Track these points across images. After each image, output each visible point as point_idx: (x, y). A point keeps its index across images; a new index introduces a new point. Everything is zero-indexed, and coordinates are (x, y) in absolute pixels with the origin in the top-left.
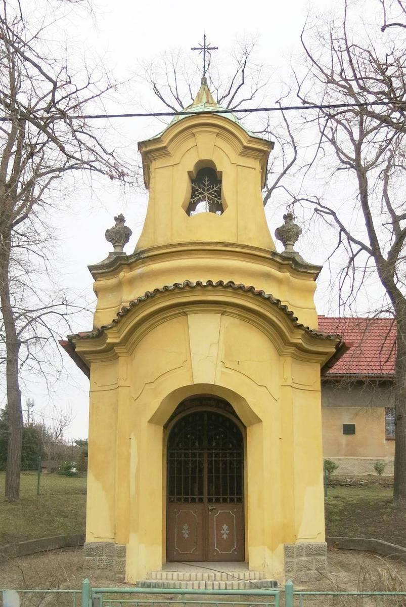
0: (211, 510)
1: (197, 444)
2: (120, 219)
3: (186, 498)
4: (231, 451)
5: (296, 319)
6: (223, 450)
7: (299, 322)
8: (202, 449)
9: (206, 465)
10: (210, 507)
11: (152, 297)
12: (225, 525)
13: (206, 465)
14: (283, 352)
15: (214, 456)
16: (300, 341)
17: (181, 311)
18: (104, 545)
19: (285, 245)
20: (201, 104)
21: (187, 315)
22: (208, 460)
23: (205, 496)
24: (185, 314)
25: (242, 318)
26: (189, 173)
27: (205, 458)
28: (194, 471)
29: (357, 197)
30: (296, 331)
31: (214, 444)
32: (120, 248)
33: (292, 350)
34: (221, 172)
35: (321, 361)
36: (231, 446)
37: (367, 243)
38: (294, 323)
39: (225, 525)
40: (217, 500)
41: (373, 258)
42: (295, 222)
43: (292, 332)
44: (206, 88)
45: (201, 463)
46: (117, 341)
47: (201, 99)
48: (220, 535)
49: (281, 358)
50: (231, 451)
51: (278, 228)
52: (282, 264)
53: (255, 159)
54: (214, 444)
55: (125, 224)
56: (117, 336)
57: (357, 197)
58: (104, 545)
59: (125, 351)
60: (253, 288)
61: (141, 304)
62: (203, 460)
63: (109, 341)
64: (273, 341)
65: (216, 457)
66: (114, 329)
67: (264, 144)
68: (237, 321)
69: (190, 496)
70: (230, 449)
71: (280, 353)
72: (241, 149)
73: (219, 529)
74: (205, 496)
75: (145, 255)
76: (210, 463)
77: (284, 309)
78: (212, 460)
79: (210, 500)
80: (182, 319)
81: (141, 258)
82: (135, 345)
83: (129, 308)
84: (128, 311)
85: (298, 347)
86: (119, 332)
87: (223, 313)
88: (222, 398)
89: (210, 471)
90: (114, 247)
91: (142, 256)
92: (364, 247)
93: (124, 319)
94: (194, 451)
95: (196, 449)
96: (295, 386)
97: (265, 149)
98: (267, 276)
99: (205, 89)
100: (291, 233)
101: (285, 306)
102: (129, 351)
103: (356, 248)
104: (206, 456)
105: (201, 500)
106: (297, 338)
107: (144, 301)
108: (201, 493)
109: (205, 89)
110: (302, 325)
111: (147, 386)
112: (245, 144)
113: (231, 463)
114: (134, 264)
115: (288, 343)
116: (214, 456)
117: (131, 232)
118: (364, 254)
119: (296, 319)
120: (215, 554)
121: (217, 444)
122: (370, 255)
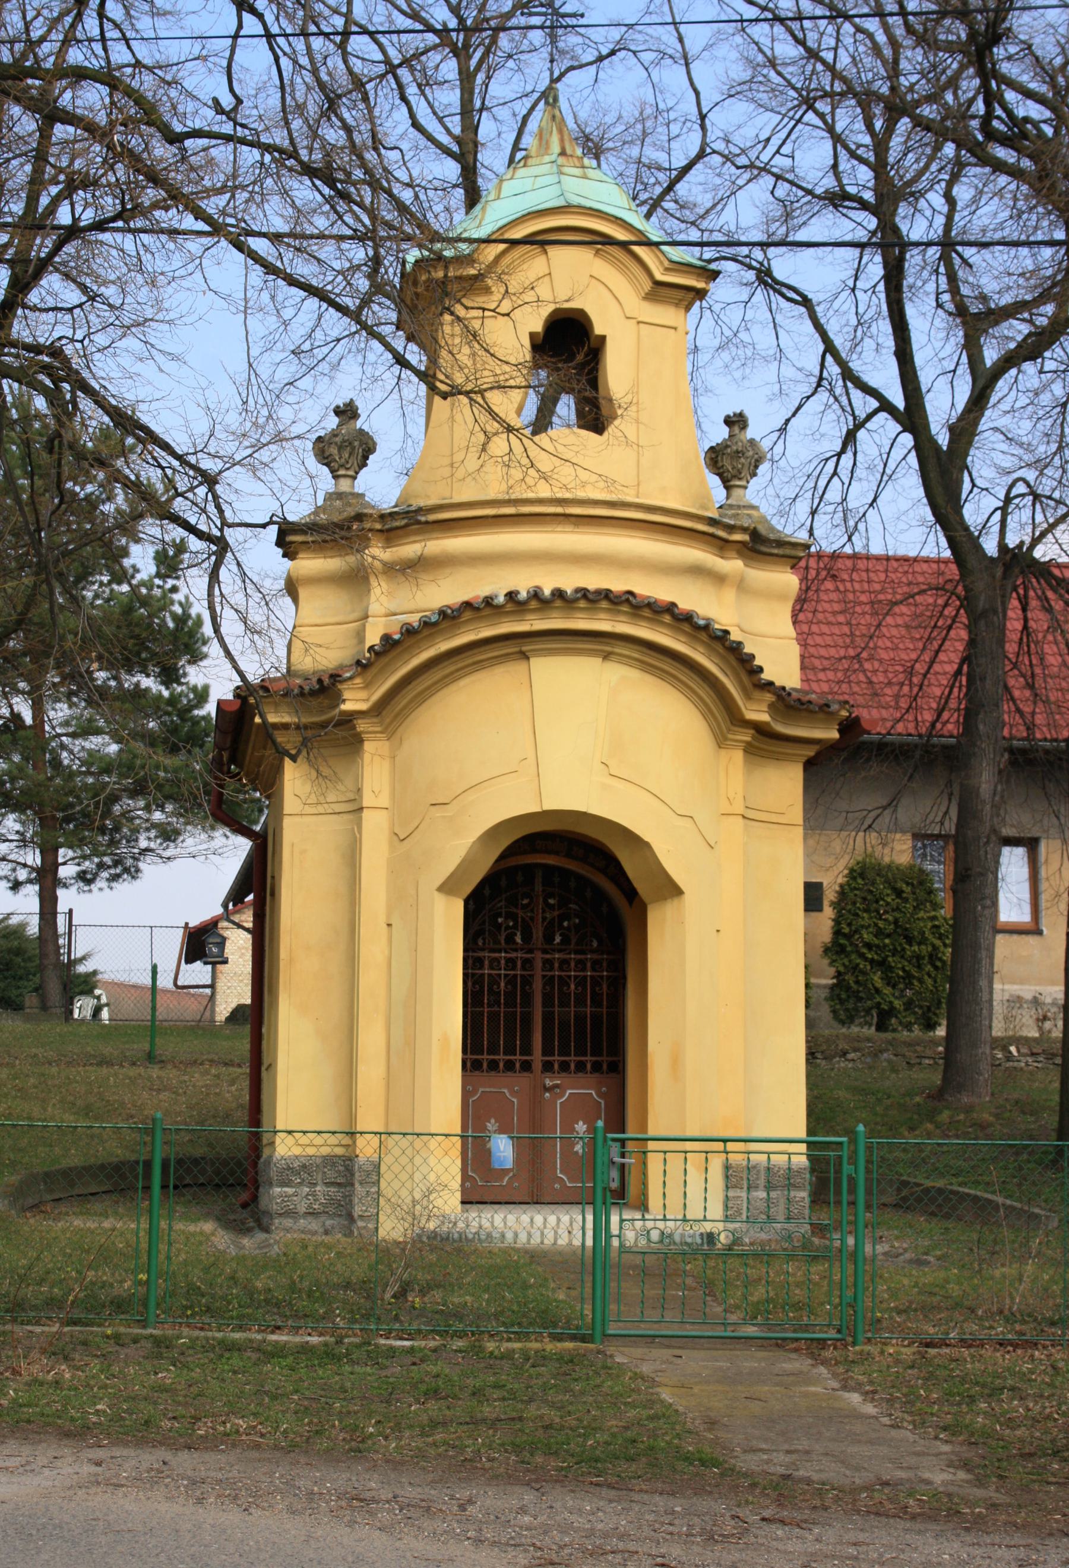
0: (547, 1089)
1: (518, 939)
2: (347, 412)
3: (509, 1061)
4: (595, 956)
5: (761, 669)
6: (576, 952)
7: (766, 676)
8: (530, 951)
9: (538, 986)
10: (548, 1083)
11: (454, 618)
12: (581, 1123)
13: (538, 986)
14: (726, 739)
15: (556, 965)
16: (765, 717)
17: (517, 649)
18: (319, 1161)
19: (728, 488)
20: (547, 159)
21: (528, 658)
22: (544, 976)
23: (537, 1057)
24: (525, 656)
25: (647, 668)
26: (532, 336)
27: (538, 972)
28: (510, 996)
29: (875, 286)
30: (757, 694)
31: (558, 939)
32: (348, 481)
33: (746, 736)
34: (603, 339)
35: (804, 759)
36: (595, 944)
37: (898, 401)
38: (755, 678)
39: (581, 1123)
40: (564, 1067)
41: (907, 439)
42: (751, 433)
43: (748, 696)
44: (557, 113)
45: (527, 981)
46: (363, 706)
47: (547, 142)
48: (568, 1143)
49: (723, 752)
50: (595, 956)
51: (712, 448)
52: (726, 541)
53: (677, 305)
54: (558, 939)
55: (359, 424)
56: (363, 694)
57: (875, 286)
58: (319, 1161)
59: (379, 729)
60: (674, 605)
61: (426, 632)
62: (532, 976)
63: (344, 707)
64: (707, 714)
65: (523, 968)
66: (358, 680)
67: (699, 275)
68: (634, 674)
69: (486, 1057)
70: (592, 951)
71: (721, 741)
72: (647, 285)
73: (569, 1127)
74: (537, 1057)
75: (432, 517)
76: (549, 981)
77: (736, 649)
78: (515, 976)
79: (548, 1067)
80: (517, 668)
81: (419, 522)
82: (402, 716)
83: (397, 637)
84: (397, 643)
85: (761, 730)
86: (367, 686)
87: (607, 656)
88: (603, 844)
89: (547, 1000)
90: (335, 477)
91: (423, 519)
92: (885, 406)
93: (384, 660)
94: (513, 955)
95: (516, 950)
96: (750, 814)
97: (700, 285)
98: (697, 571)
99: (554, 117)
100: (742, 460)
101: (740, 643)
102: (386, 728)
103: (864, 404)
104: (538, 964)
105: (527, 1067)
106: (758, 712)
107: (435, 624)
108: (527, 1050)
109: (554, 117)
110: (771, 684)
111: (437, 812)
112: (660, 277)
113: (564, 982)
114: (399, 532)
115: (737, 719)
116: (556, 965)
117: (375, 444)
118: (885, 426)
119: (761, 669)
120: (557, 1186)
121: (565, 940)
122: (899, 428)
